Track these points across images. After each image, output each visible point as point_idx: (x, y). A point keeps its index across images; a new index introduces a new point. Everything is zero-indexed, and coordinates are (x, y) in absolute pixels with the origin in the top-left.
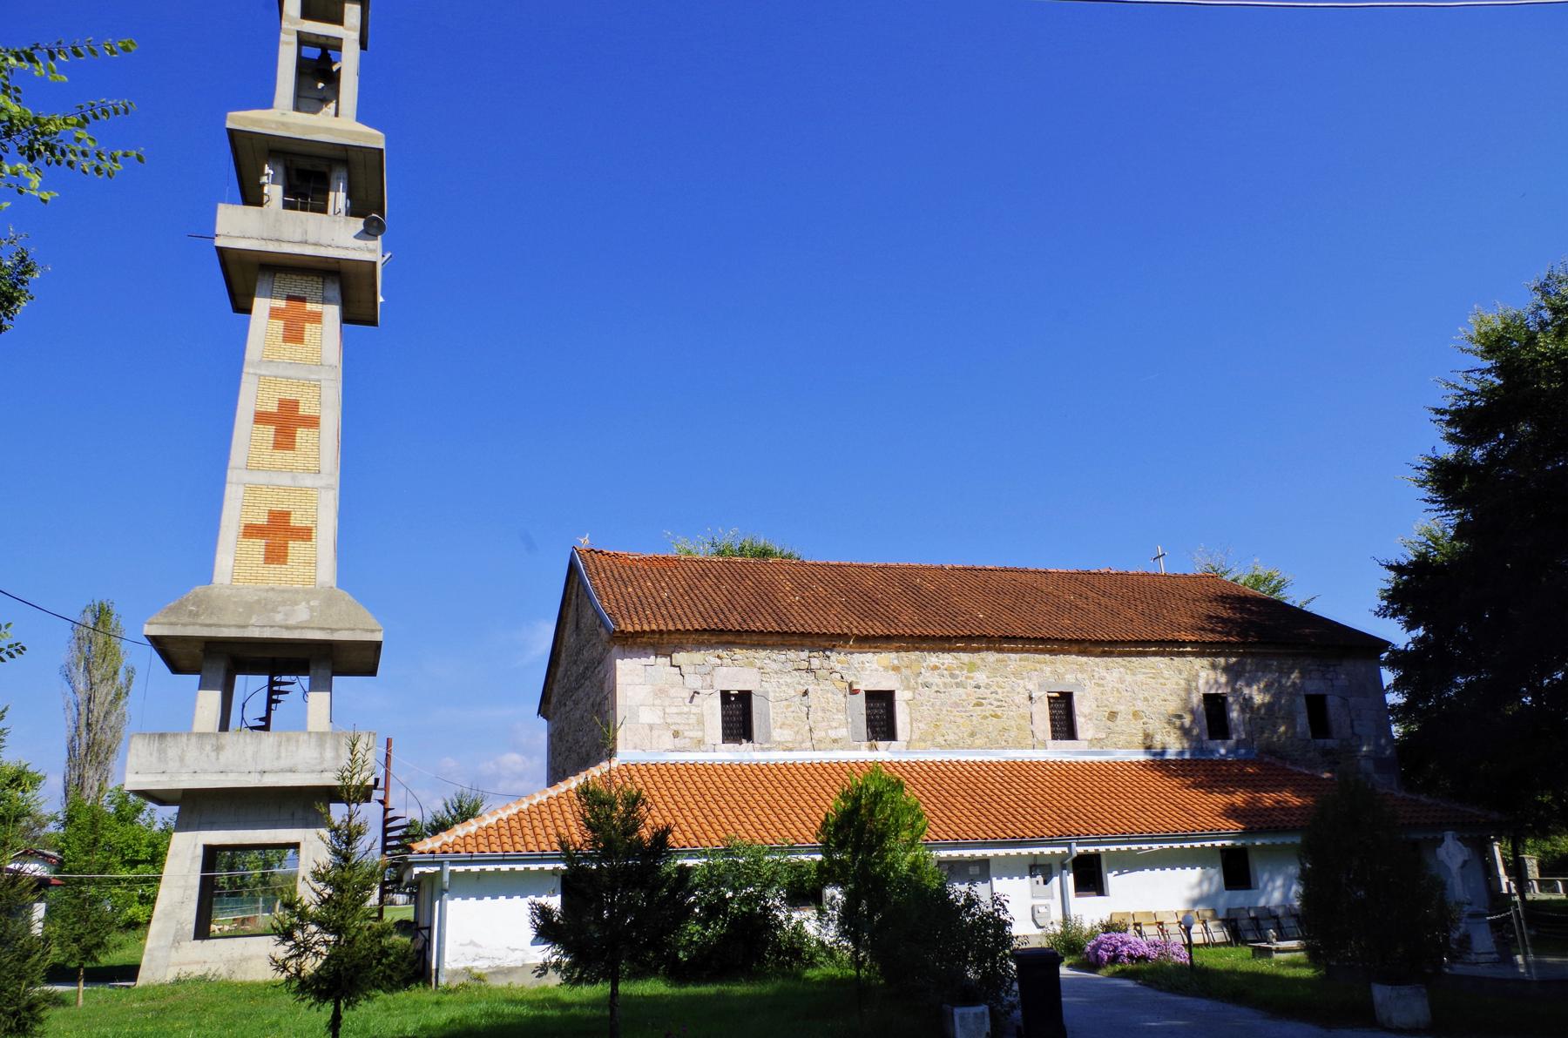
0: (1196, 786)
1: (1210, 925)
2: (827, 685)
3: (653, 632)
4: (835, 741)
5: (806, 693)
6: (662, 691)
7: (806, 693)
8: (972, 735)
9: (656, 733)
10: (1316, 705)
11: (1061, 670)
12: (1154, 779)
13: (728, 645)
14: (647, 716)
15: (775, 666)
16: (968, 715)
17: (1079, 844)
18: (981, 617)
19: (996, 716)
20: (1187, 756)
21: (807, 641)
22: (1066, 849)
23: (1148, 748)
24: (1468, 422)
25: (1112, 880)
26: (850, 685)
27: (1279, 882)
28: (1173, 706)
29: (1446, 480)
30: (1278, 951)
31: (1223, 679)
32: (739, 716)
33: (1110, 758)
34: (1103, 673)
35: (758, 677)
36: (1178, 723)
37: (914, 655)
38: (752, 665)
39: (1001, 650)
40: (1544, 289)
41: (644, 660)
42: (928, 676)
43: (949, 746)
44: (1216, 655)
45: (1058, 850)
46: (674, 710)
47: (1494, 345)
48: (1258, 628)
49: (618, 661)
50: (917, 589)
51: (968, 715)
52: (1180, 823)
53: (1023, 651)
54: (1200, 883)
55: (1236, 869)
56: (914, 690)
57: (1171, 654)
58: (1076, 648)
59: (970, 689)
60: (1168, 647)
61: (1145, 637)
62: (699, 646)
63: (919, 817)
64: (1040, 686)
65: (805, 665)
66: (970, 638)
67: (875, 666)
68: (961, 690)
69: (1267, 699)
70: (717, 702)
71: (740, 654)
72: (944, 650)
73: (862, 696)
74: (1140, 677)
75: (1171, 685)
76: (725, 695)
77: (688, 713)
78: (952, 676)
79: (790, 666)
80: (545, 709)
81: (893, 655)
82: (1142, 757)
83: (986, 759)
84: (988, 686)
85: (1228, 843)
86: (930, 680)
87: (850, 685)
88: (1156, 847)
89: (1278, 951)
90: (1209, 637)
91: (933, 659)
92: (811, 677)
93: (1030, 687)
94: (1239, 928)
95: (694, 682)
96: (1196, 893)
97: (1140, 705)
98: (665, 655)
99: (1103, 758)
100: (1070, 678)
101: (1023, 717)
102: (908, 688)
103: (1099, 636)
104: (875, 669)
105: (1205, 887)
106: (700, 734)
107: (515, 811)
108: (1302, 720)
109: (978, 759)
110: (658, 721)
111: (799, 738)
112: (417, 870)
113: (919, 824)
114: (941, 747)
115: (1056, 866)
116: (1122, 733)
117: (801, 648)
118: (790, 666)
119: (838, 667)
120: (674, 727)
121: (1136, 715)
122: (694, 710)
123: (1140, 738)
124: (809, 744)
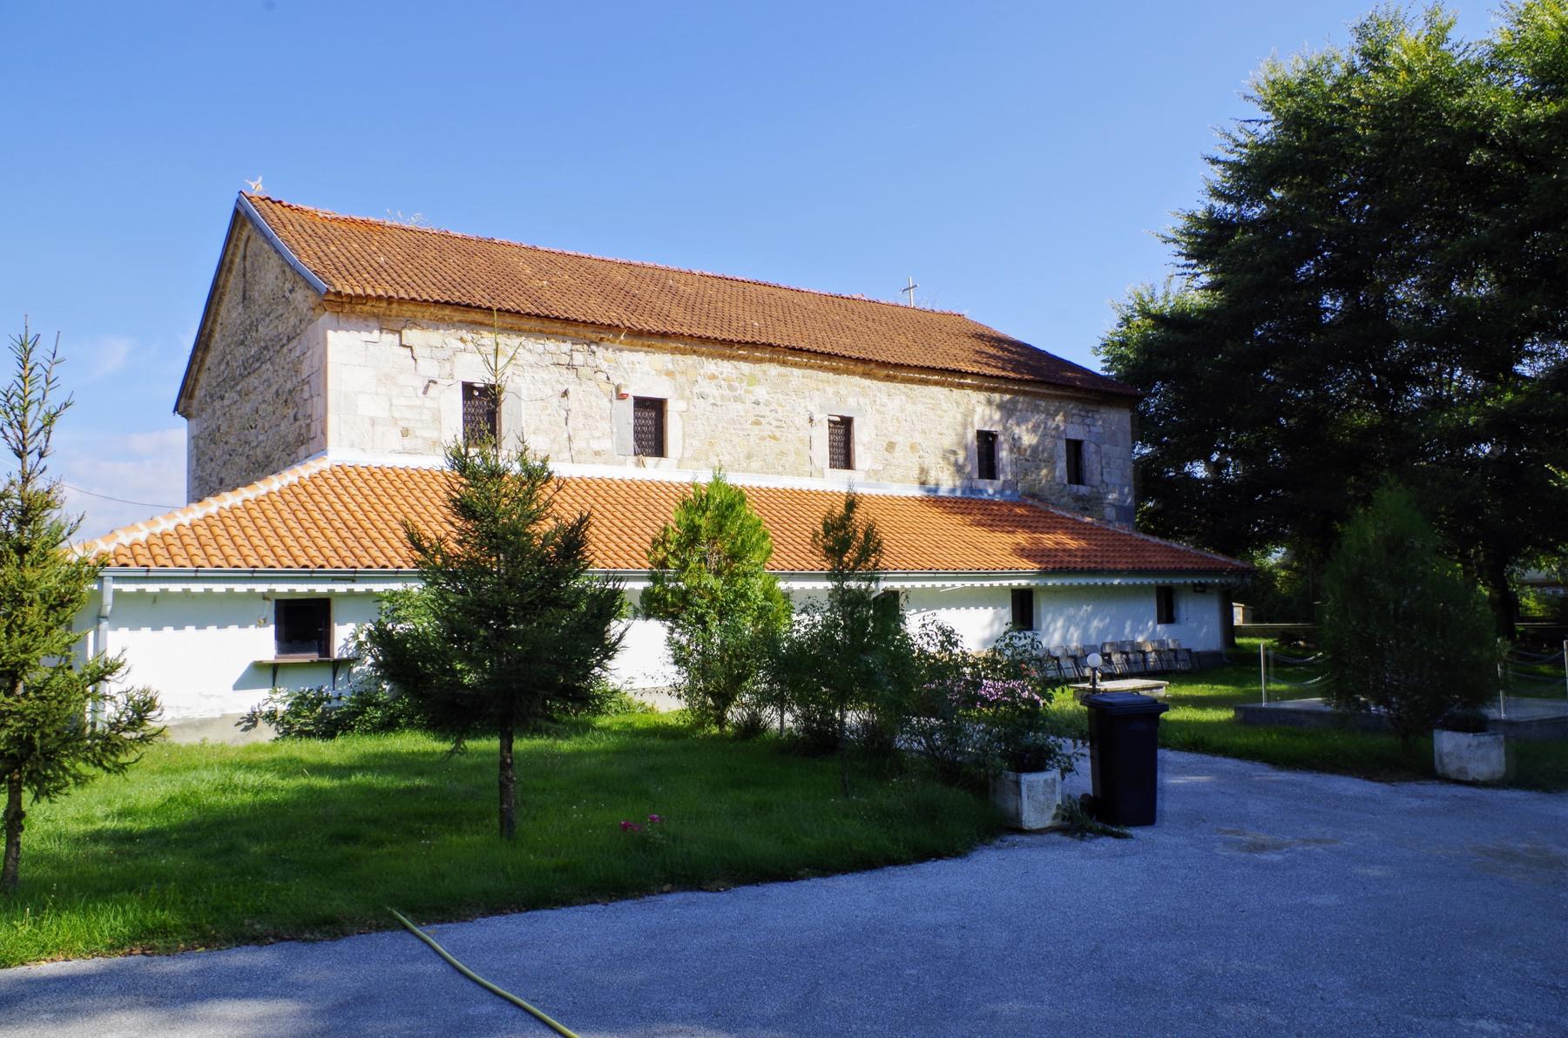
0: (979, 524)
3: (379, 298)
4: (597, 453)
5: (565, 394)
7: (565, 394)
8: (749, 457)
10: (1075, 448)
11: (843, 392)
12: (936, 517)
15: (531, 358)
16: (752, 434)
18: (755, 326)
19: (775, 438)
20: (958, 494)
21: (571, 330)
23: (923, 483)
24: (1254, 172)
26: (618, 389)
27: (1060, 623)
28: (949, 441)
31: (997, 416)
32: (651, 425)
34: (885, 399)
36: (952, 459)
37: (691, 360)
39: (784, 363)
41: (365, 335)
44: (993, 390)
48: (1031, 374)
49: (331, 334)
52: (984, 564)
53: (807, 366)
54: (992, 624)
55: (1023, 608)
56: (688, 400)
57: (951, 385)
58: (860, 368)
59: (749, 405)
60: (949, 376)
61: (928, 364)
62: (438, 323)
65: (565, 360)
68: (739, 406)
72: (723, 357)
73: (631, 402)
76: (468, 388)
78: (731, 388)
79: (547, 360)
80: (185, 403)
81: (668, 357)
84: (768, 403)
85: (1024, 583)
86: (707, 390)
87: (618, 389)
88: (958, 584)
92: (572, 375)
93: (812, 408)
95: (429, 368)
97: (918, 438)
98: (392, 331)
99: (881, 492)
101: (802, 441)
102: (682, 397)
104: (646, 372)
107: (200, 515)
117: (563, 337)
118: (547, 360)
119: (604, 366)
120: (405, 424)
121: (913, 447)
122: (429, 403)
123: (916, 472)
124: (567, 455)
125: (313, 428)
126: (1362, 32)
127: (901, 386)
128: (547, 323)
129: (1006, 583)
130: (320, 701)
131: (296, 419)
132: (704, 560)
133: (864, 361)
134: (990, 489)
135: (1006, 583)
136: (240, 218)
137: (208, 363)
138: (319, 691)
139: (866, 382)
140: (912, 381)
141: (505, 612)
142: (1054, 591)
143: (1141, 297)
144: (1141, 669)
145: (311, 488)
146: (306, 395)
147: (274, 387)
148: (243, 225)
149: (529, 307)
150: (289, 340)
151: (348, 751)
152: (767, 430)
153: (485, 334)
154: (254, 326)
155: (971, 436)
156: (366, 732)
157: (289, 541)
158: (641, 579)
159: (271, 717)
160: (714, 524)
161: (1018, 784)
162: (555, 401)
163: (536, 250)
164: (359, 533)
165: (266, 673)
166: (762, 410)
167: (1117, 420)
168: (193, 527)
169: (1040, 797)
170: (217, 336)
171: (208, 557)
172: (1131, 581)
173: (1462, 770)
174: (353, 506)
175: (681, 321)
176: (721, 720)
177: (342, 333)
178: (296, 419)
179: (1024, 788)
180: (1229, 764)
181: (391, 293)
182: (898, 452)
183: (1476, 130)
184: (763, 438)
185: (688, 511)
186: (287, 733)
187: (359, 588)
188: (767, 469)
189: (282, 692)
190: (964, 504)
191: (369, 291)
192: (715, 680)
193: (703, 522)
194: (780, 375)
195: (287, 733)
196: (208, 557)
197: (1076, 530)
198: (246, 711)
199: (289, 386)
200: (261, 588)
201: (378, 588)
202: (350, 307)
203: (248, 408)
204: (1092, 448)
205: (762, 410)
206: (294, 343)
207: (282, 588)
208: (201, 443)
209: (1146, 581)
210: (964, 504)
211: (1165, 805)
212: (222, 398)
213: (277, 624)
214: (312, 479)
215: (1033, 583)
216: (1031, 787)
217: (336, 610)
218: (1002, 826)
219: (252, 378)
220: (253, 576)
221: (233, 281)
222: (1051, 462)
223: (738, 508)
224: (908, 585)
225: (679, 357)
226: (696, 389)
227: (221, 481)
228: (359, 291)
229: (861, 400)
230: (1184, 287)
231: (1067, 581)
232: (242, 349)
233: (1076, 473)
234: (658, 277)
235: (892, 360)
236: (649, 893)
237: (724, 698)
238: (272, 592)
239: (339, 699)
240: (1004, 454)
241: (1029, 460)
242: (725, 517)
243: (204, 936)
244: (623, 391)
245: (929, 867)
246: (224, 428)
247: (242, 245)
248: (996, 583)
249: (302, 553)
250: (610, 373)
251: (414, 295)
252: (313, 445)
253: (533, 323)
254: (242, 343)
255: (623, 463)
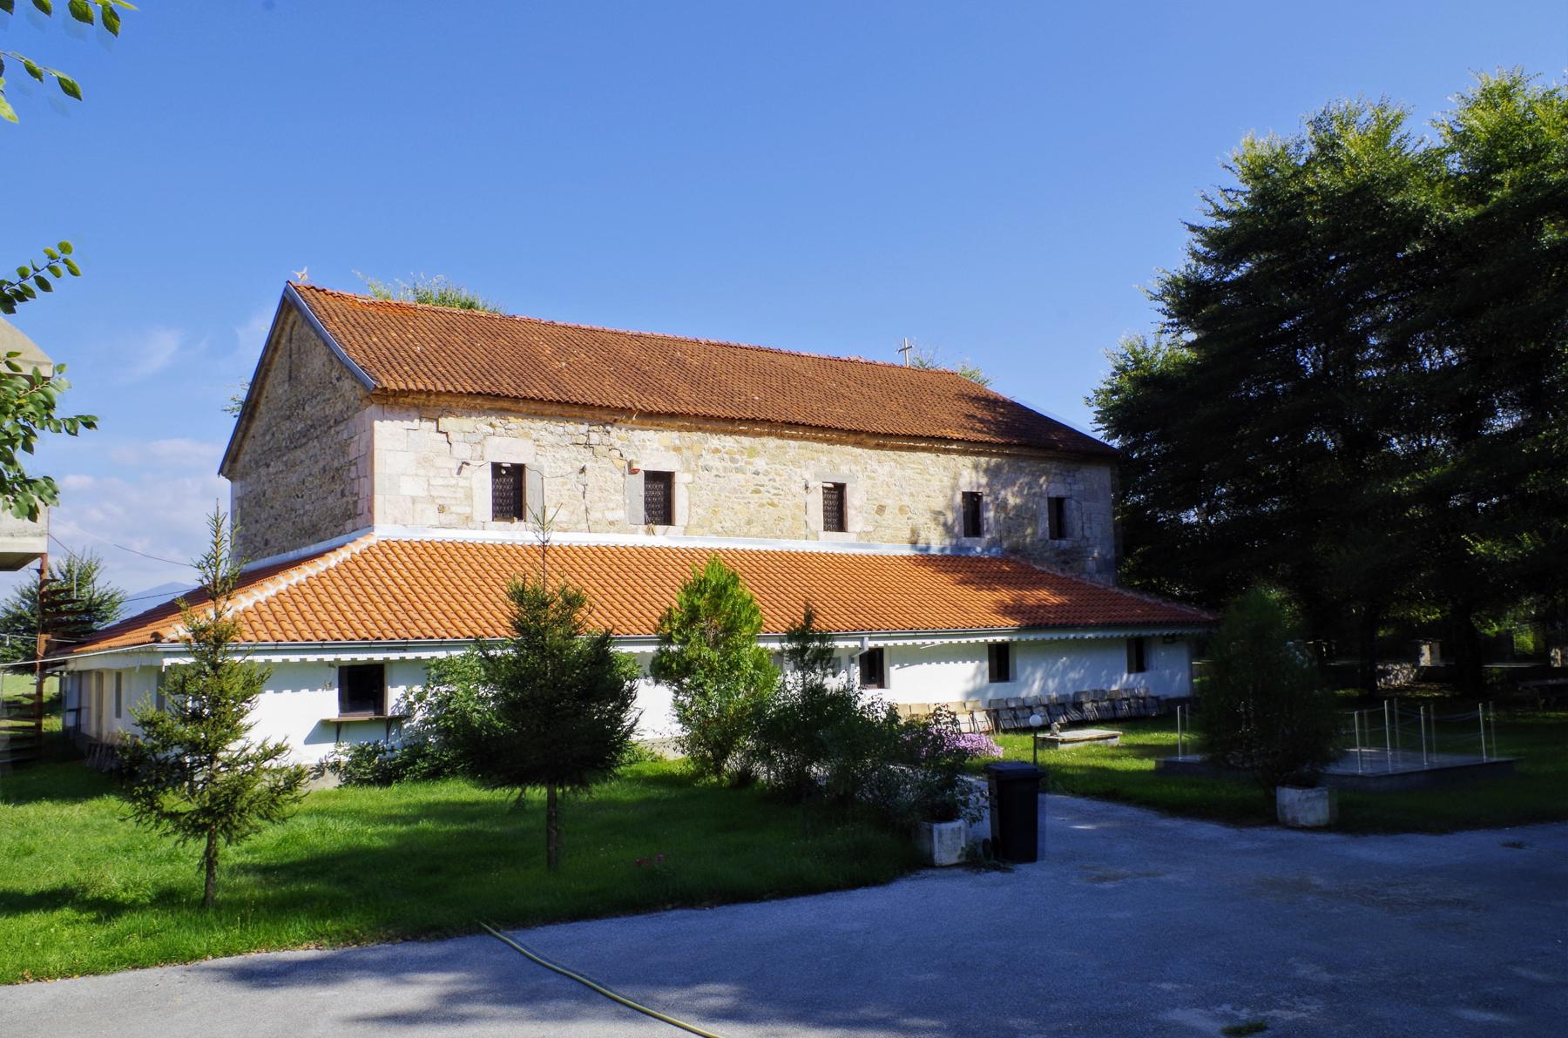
0: (963, 582)
1: (976, 715)
2: (606, 463)
3: (420, 391)
4: (612, 523)
5: (583, 470)
6: (426, 460)
7: (583, 470)
8: (749, 523)
9: (419, 507)
10: (1057, 506)
11: (837, 461)
12: (926, 575)
13: (503, 412)
14: (410, 487)
15: (551, 439)
16: (749, 502)
17: (871, 639)
18: (755, 400)
19: (772, 505)
20: (948, 552)
21: (588, 414)
22: (858, 643)
23: (914, 543)
24: (1225, 245)
25: (894, 673)
26: (630, 464)
27: (1039, 675)
28: (939, 503)
29: (1189, 300)
30: (1063, 742)
31: (984, 481)
32: (660, 499)
33: (878, 552)
34: (876, 466)
35: (534, 449)
36: (942, 519)
37: (697, 436)
38: (527, 436)
39: (782, 436)
40: (1317, 124)
41: (407, 424)
42: (709, 459)
43: (726, 533)
44: (978, 454)
45: (851, 644)
46: (440, 482)
47: (1258, 172)
48: (1020, 434)
49: (377, 424)
50: (681, 364)
51: (749, 502)
52: (958, 620)
53: (802, 438)
54: (975, 676)
55: (1000, 662)
56: (694, 472)
57: (938, 451)
58: (852, 438)
59: (749, 475)
60: (936, 443)
61: (915, 432)
62: (470, 411)
63: (755, 611)
64: (817, 476)
65: (583, 439)
66: (754, 421)
67: (656, 445)
68: (740, 476)
69: (1018, 501)
70: (487, 475)
71: (514, 422)
72: (726, 432)
73: (641, 475)
74: (909, 472)
75: (936, 484)
76: (496, 468)
77: (457, 485)
78: (733, 460)
79: (567, 440)
80: (230, 465)
81: (675, 434)
82: (908, 551)
83: (762, 548)
84: (766, 473)
85: (999, 639)
86: (711, 463)
87: (630, 464)
88: (937, 642)
89: (1063, 742)
90: (973, 436)
91: (715, 441)
92: (588, 453)
93: (807, 476)
94: (1006, 717)
95: (462, 451)
96: (970, 686)
97: (907, 501)
98: (430, 419)
99: (871, 552)
100: (844, 469)
101: (798, 507)
102: (688, 470)
103: (875, 427)
104: (655, 448)
105: (979, 680)
106: (468, 510)
107: (273, 592)
108: (1044, 525)
109: (755, 548)
110: (423, 494)
111: (575, 518)
112: (167, 662)
113: (756, 619)
114: (717, 533)
115: (844, 661)
116: (888, 527)
117: (580, 420)
118: (567, 440)
120: (440, 501)
121: (901, 509)
122: (462, 483)
123: (908, 534)
124: (584, 526)
125: (360, 505)
126: (1317, 124)
127: (891, 453)
128: (567, 409)
129: (981, 640)
130: (376, 753)
131: (343, 495)
132: (703, 633)
133: (856, 432)
134: (978, 547)
135: (981, 640)
136: (288, 305)
137: (252, 431)
138: (376, 744)
139: (859, 451)
140: (901, 448)
141: (551, 701)
142: (1028, 644)
143: (1134, 352)
144: (1110, 715)
145: (363, 564)
146: (353, 475)
147: (321, 464)
148: (289, 311)
149: (551, 394)
150: (337, 423)
151: (404, 800)
152: (765, 497)
153: (512, 419)
154: (301, 404)
155: (959, 498)
156: (415, 780)
157: (350, 615)
158: (652, 643)
159: (335, 767)
160: (709, 610)
161: (931, 831)
162: (573, 477)
163: (553, 324)
164: (407, 606)
165: (330, 731)
166: (761, 479)
167: (1099, 478)
168: (268, 603)
169: (949, 840)
170: (262, 408)
171: (284, 631)
172: (1101, 634)
173: (1295, 820)
174: (400, 581)
175: (687, 400)
176: (718, 770)
177: (387, 423)
178: (343, 495)
179: (936, 835)
180: (1127, 812)
181: (431, 387)
182: (887, 515)
183: (1413, 222)
184: (762, 505)
185: (688, 594)
186: (348, 782)
187: (410, 656)
188: (767, 533)
189: (346, 746)
190: (952, 562)
191: (412, 386)
192: (711, 737)
193: (701, 602)
194: (778, 447)
195: (348, 782)
196: (284, 631)
197: (1058, 586)
198: (314, 762)
199: (336, 464)
200: (329, 658)
201: (425, 655)
202: (396, 401)
203: (294, 479)
204: (1073, 504)
205: (761, 479)
206: (342, 427)
207: (346, 657)
208: (245, 505)
209: (1116, 634)
210: (952, 562)
211: (1048, 843)
212: (268, 466)
213: (340, 686)
214: (362, 554)
215: (1015, 639)
216: (940, 835)
217: (389, 674)
218: (919, 863)
219: (298, 452)
220: (322, 648)
221: (280, 360)
222: (1034, 518)
223: (730, 589)
224: (890, 643)
225: (685, 434)
226: (701, 463)
227: (267, 543)
228: (403, 386)
229: (854, 468)
230: (1166, 342)
231: (1047, 636)
232: (288, 424)
233: (1059, 526)
234: (665, 348)
235: (881, 430)
236: (657, 910)
237: (723, 749)
238: (337, 660)
239: (392, 750)
240: (990, 515)
241: (1021, 516)
242: (719, 597)
243: (354, 937)
244: (635, 466)
245: (859, 892)
246: (269, 493)
247: (288, 328)
248: (973, 640)
249: (361, 629)
250: (623, 450)
251: (450, 388)
252: (360, 521)
253: (554, 409)
254: (289, 418)
255: (634, 532)
